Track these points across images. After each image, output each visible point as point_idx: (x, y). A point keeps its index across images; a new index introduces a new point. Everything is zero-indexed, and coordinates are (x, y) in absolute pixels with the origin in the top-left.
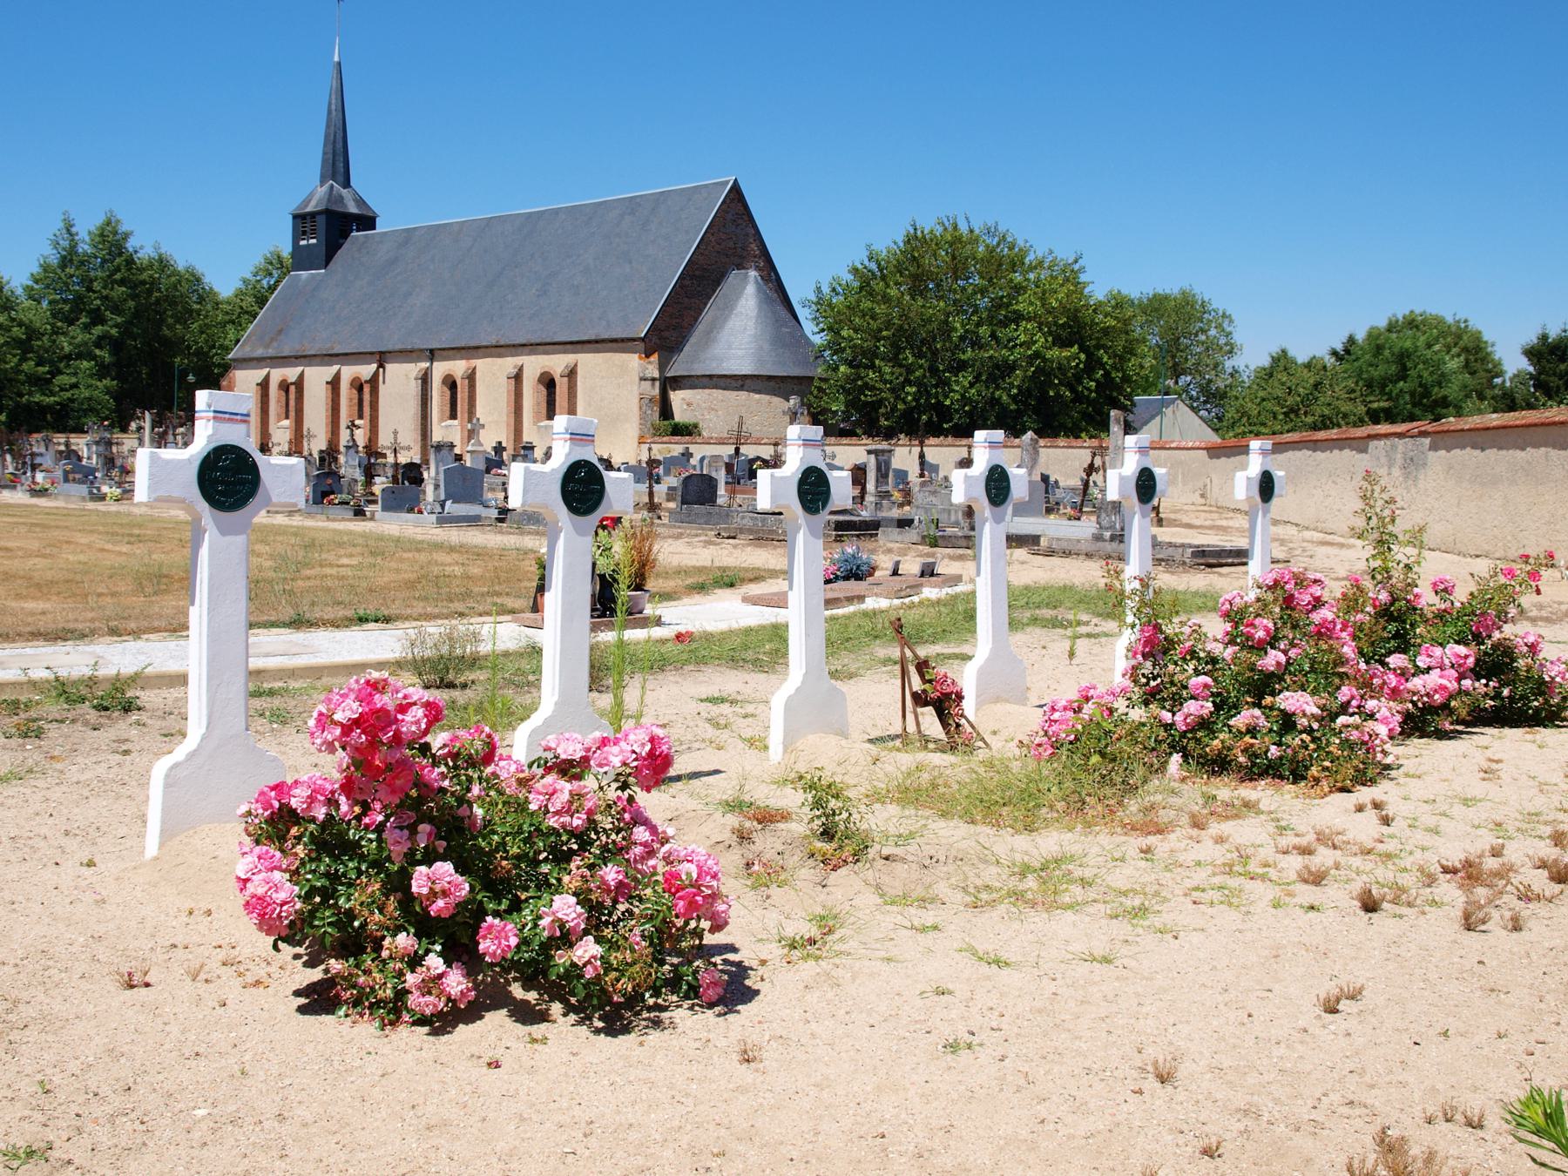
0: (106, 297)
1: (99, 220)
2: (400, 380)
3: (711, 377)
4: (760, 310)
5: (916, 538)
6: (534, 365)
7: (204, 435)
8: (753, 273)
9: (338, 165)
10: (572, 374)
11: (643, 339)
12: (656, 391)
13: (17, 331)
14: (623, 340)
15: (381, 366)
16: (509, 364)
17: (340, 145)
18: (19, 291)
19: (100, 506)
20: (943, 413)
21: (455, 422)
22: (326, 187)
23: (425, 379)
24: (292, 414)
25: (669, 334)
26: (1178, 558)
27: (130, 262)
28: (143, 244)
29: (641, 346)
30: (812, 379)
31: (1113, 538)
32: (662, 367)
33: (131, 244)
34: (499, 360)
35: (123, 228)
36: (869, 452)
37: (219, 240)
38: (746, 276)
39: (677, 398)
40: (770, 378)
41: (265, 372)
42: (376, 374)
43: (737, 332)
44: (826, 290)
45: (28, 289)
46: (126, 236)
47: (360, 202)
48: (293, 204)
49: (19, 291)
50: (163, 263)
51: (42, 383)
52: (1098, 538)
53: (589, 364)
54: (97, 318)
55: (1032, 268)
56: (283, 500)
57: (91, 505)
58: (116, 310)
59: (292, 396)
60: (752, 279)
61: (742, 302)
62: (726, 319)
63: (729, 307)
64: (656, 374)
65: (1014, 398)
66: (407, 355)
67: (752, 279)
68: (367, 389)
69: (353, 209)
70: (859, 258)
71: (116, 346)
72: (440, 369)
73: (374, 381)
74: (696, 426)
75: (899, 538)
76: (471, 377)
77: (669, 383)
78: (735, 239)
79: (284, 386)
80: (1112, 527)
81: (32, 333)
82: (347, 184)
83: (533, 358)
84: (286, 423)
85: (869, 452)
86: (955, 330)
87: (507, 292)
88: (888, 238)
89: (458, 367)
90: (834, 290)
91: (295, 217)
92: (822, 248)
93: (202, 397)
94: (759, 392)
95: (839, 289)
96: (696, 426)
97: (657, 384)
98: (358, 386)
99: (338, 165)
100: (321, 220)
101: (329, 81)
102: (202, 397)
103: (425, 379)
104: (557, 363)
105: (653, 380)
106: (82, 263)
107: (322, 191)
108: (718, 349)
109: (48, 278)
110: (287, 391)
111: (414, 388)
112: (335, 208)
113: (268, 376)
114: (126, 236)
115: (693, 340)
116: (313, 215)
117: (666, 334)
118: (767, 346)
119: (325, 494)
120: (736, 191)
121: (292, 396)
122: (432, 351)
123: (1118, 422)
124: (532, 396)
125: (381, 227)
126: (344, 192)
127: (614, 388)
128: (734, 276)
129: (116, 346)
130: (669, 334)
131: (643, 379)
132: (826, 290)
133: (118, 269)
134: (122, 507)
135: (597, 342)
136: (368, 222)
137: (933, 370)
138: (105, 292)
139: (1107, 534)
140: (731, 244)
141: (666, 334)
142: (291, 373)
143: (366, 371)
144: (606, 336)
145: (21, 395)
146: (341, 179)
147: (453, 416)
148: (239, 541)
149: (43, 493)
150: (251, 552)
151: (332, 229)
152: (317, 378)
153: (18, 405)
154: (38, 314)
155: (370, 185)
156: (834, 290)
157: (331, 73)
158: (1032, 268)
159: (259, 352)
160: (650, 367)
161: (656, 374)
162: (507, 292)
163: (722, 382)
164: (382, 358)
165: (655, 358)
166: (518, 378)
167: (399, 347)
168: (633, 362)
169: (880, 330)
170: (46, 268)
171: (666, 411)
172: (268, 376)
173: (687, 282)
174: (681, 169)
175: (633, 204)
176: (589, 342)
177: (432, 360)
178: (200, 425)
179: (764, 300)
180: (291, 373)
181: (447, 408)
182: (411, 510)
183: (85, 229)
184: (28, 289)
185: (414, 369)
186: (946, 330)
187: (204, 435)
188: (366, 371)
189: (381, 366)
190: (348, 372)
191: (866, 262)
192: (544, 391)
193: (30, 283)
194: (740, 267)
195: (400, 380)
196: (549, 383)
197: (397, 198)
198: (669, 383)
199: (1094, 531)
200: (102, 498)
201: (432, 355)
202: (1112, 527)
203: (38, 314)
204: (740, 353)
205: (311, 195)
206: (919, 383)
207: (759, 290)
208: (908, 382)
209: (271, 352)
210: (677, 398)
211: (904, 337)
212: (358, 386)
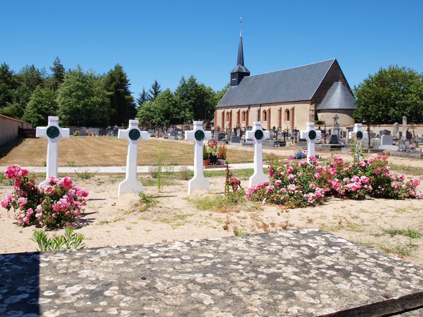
0: (191, 94)
1: (190, 77)
2: (253, 111)
3: (328, 109)
4: (342, 92)
5: (350, 150)
6: (284, 107)
7: (130, 127)
8: (340, 83)
9: (241, 61)
10: (293, 109)
11: (310, 100)
12: (314, 113)
13: (173, 102)
14: (306, 101)
15: (249, 108)
16: (278, 107)
17: (241, 56)
18: (173, 93)
19: (176, 141)
20: (389, 118)
21: (266, 121)
22: (238, 66)
23: (259, 111)
24: (229, 120)
25: (318, 99)
26: (417, 156)
27: (196, 86)
28: (199, 82)
29: (310, 102)
30: (354, 109)
31: (403, 151)
32: (315, 107)
33: (196, 82)
34: (276, 106)
35: (194, 78)
36: (347, 128)
37: (215, 80)
38: (338, 84)
39: (320, 115)
40: (344, 109)
41: (223, 110)
42: (248, 110)
43: (336, 98)
44: (357, 86)
45: (175, 93)
46: (196, 79)
47: (246, 69)
48: (231, 71)
49: (173, 93)
50: (203, 86)
51: (178, 113)
52: (399, 151)
53: (297, 106)
54: (189, 99)
55: (416, 78)
56: (65, 136)
57: (175, 141)
58: (193, 97)
59: (246, 116)
60: (340, 84)
61: (337, 90)
62: (332, 94)
63: (333, 91)
64: (314, 109)
65: (409, 113)
66: (255, 105)
67: (340, 84)
68: (246, 114)
69: (244, 71)
70: (367, 77)
71: (194, 104)
72: (262, 109)
73: (247, 112)
74: (324, 122)
75: (346, 150)
76: (269, 111)
77: (317, 111)
78: (335, 75)
79: (228, 113)
80: (402, 148)
81: (176, 102)
82: (243, 65)
83: (284, 106)
84: (228, 122)
85: (347, 128)
86: (392, 95)
87: (278, 90)
88: (374, 72)
89: (266, 108)
90: (359, 86)
91: (231, 74)
92: (357, 76)
93: (130, 121)
94: (341, 113)
95: (361, 85)
96: (324, 122)
97: (314, 111)
98: (244, 113)
99: (241, 61)
100: (237, 74)
101: (239, 41)
102: (130, 121)
103: (259, 111)
104: (289, 107)
105: (313, 110)
106: (186, 86)
107: (237, 67)
108: (330, 102)
109: (179, 90)
110: (244, 114)
111: (256, 113)
112: (240, 71)
113: (240, 110)
114: (196, 79)
115: (324, 100)
116: (235, 73)
117: (317, 99)
118: (343, 101)
119: (221, 138)
120: (336, 63)
121: (246, 116)
122: (261, 104)
123: (405, 119)
124: (284, 115)
125: (251, 75)
126: (242, 67)
127: (303, 113)
128: (335, 83)
129: (194, 104)
130: (318, 99)
131: (310, 110)
132: (357, 86)
133: (194, 87)
134: (182, 142)
135: (299, 101)
136: (248, 74)
137: (386, 107)
138: (191, 92)
139: (401, 150)
140: (334, 75)
141: (317, 99)
142: (229, 110)
143: (246, 109)
144: (301, 100)
145: (173, 116)
146: (242, 64)
147: (265, 120)
148: (136, 145)
149: (167, 138)
150: (137, 147)
151: (239, 76)
152: (235, 111)
153: (173, 119)
154: (177, 98)
155: (248, 66)
156: (359, 86)
157: (240, 39)
158: (416, 78)
159: (222, 106)
160: (312, 107)
161: (314, 109)
162: (278, 90)
163: (331, 111)
164: (249, 106)
165: (313, 105)
166: (280, 110)
167: (253, 103)
168: (308, 106)
169: (371, 96)
170: (179, 88)
171: (316, 118)
172: (240, 110)
173: (322, 86)
174: (317, 57)
175: (310, 67)
176: (297, 101)
177: (261, 107)
178: (129, 125)
179: (343, 89)
180: (229, 110)
181: (264, 118)
182: (237, 142)
183: (187, 79)
184: (175, 93)
185: (256, 109)
186: (389, 96)
187: (130, 127)
188: (246, 109)
189: (249, 108)
190: (242, 110)
191: (368, 78)
192: (287, 113)
193: (175, 91)
194: (337, 81)
195: (253, 111)
196: (288, 112)
197: (255, 68)
198: (317, 111)
199: (398, 149)
200: (178, 139)
201: (261, 105)
202: (402, 148)
203: (177, 98)
204: (336, 103)
205: (235, 68)
206: (382, 111)
207: (342, 87)
208: (379, 110)
209: (225, 105)
210: (320, 115)
211: (378, 99)
212: (244, 113)
